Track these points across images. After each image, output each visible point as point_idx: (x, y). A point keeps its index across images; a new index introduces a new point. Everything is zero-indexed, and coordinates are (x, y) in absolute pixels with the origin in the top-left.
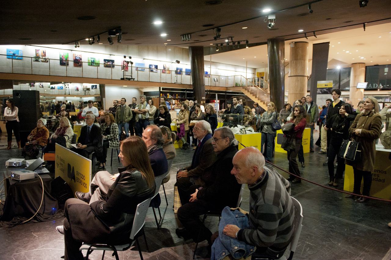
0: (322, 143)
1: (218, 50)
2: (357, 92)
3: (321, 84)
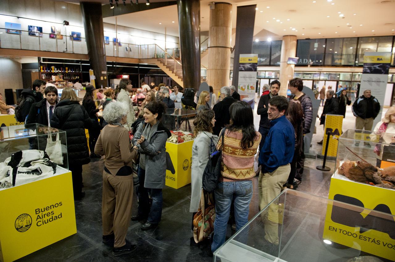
0: (226, 139)
1: (113, 7)
2: (287, 68)
3: (244, 58)
